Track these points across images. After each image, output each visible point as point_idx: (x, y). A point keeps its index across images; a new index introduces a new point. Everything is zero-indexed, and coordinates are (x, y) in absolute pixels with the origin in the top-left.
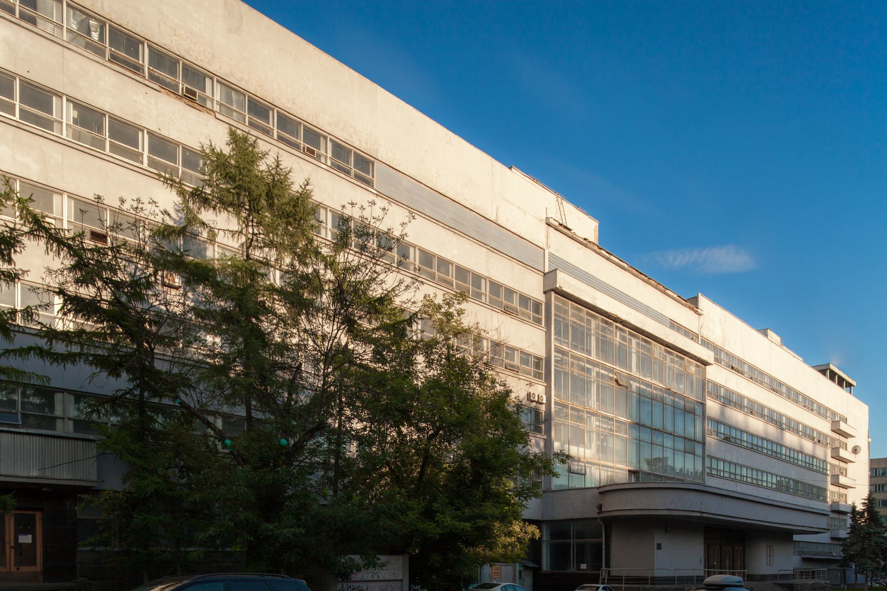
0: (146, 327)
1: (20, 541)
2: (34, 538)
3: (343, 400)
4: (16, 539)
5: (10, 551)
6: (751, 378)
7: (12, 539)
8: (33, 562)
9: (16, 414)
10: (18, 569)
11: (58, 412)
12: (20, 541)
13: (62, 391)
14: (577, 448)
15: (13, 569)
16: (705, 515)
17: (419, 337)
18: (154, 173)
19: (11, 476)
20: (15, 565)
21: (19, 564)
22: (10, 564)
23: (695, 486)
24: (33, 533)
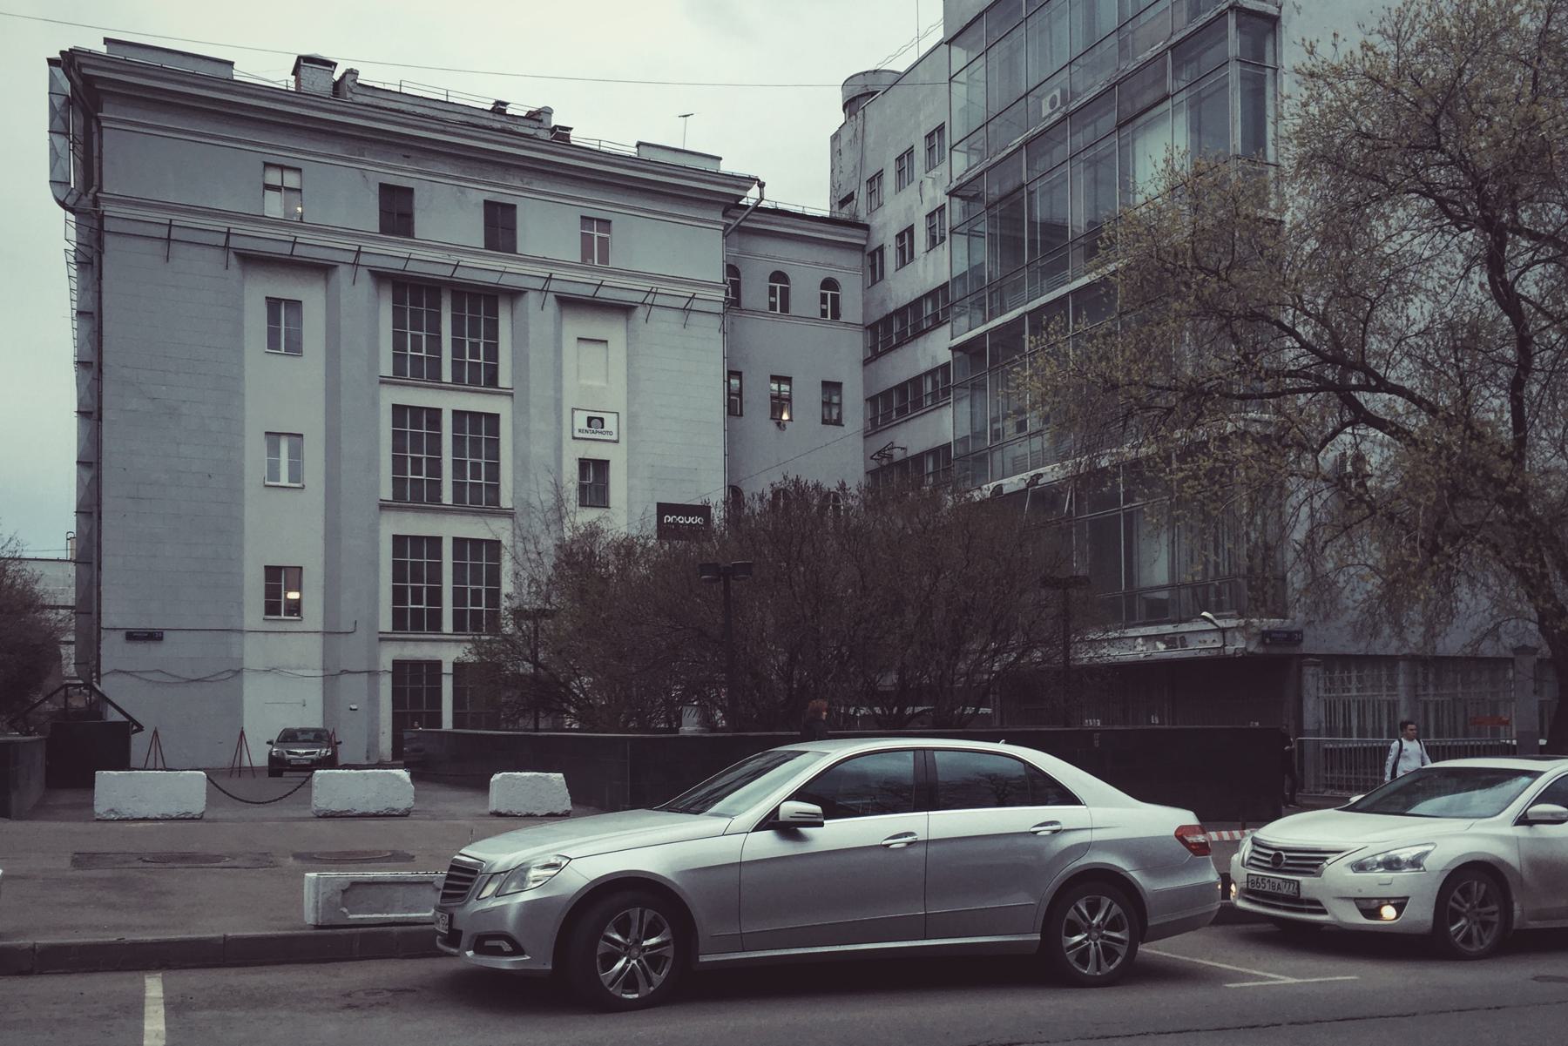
17: (72, 638)
24: (288, 600)
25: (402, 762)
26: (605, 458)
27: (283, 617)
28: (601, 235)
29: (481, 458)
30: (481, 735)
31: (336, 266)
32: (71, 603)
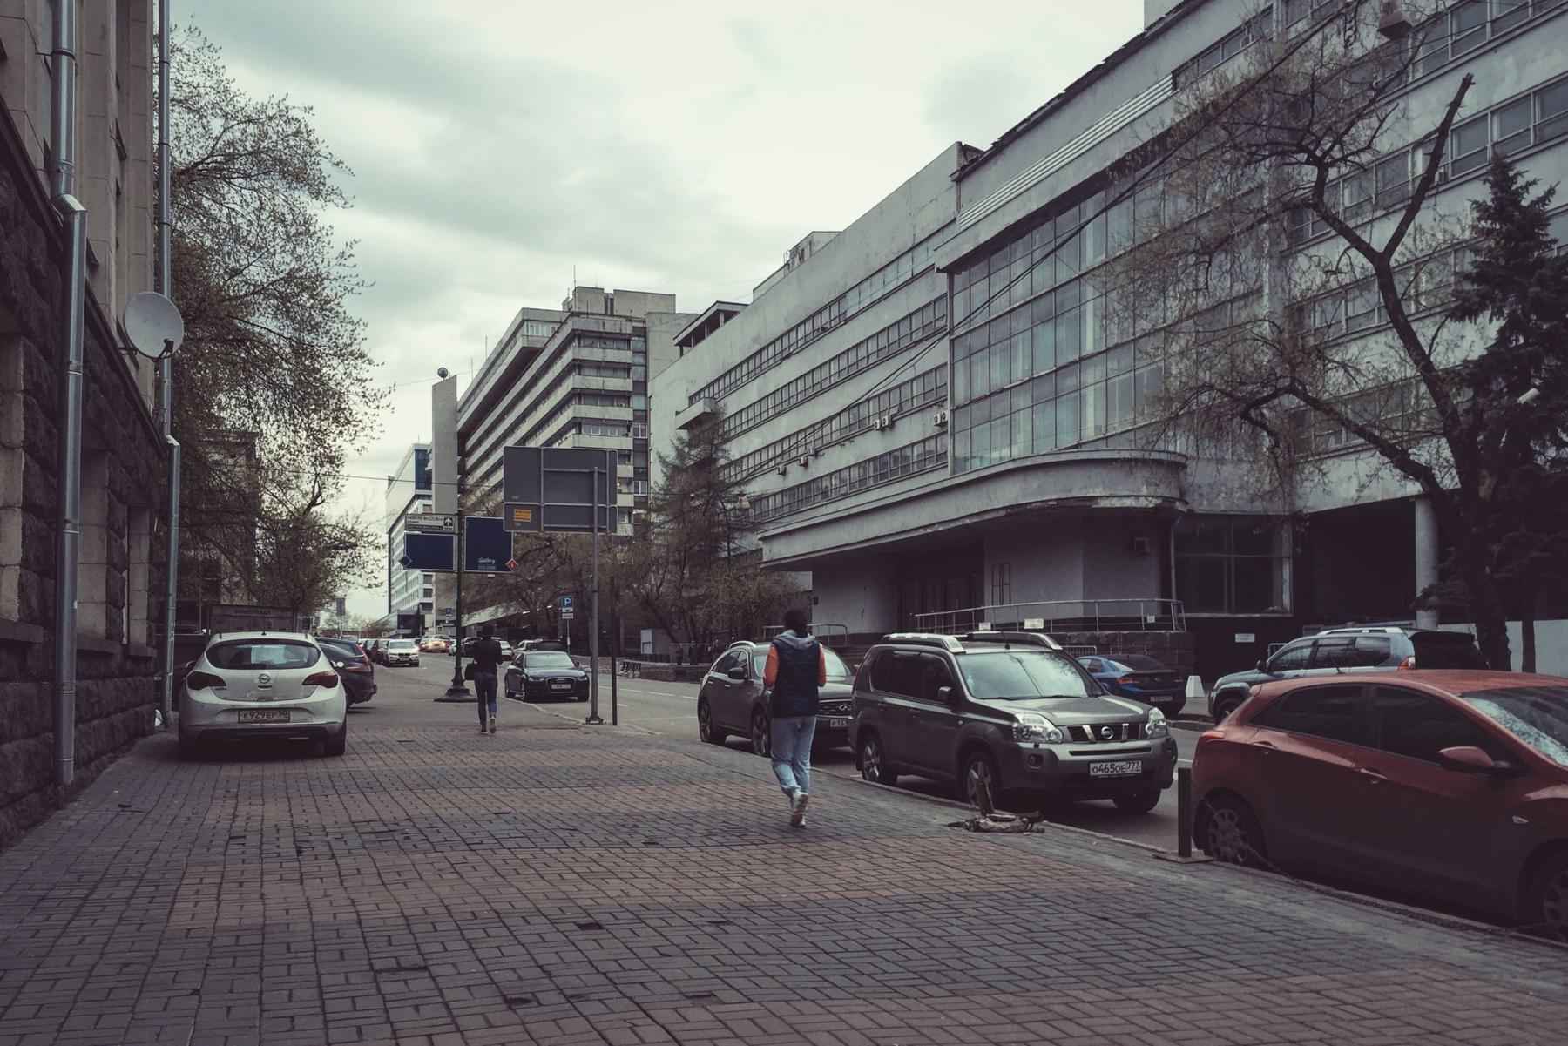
0: (874, 772)
16: (886, 787)
25: (1514, 629)
26: (430, 389)
29: (1170, 597)
30: (1169, 550)
31: (177, 246)
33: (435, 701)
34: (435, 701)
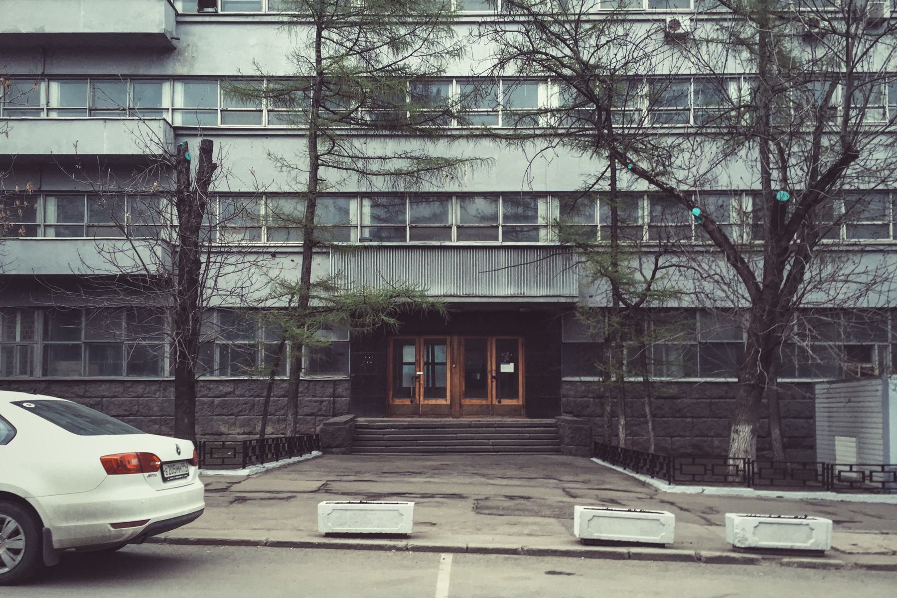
1: (502, 371)
2: (516, 368)
3: (606, 131)
4: (498, 368)
5: (492, 382)
6: (479, 530)
7: (494, 368)
8: (515, 396)
9: (497, 227)
10: (499, 402)
11: (39, 220)
12: (502, 371)
13: (544, 195)
14: (404, 366)
15: (495, 402)
18: (824, 403)
19: (485, 297)
20: (497, 397)
21: (500, 396)
22: (492, 397)
23: (485, 18)
27: (408, 242)
28: (869, 365)
32: (404, 366)
33: (13, 403)
34: (13, 403)
